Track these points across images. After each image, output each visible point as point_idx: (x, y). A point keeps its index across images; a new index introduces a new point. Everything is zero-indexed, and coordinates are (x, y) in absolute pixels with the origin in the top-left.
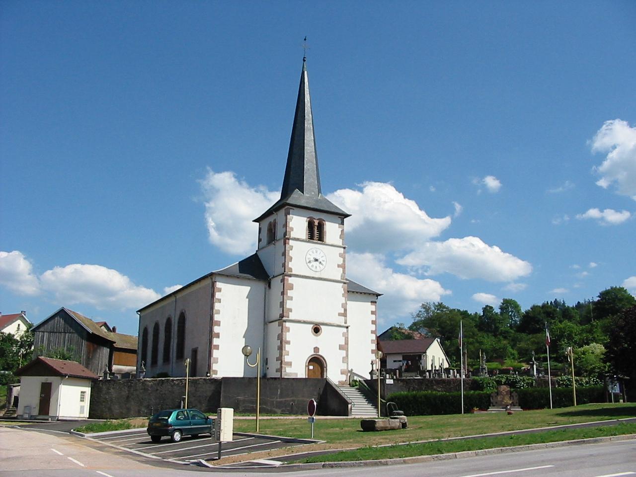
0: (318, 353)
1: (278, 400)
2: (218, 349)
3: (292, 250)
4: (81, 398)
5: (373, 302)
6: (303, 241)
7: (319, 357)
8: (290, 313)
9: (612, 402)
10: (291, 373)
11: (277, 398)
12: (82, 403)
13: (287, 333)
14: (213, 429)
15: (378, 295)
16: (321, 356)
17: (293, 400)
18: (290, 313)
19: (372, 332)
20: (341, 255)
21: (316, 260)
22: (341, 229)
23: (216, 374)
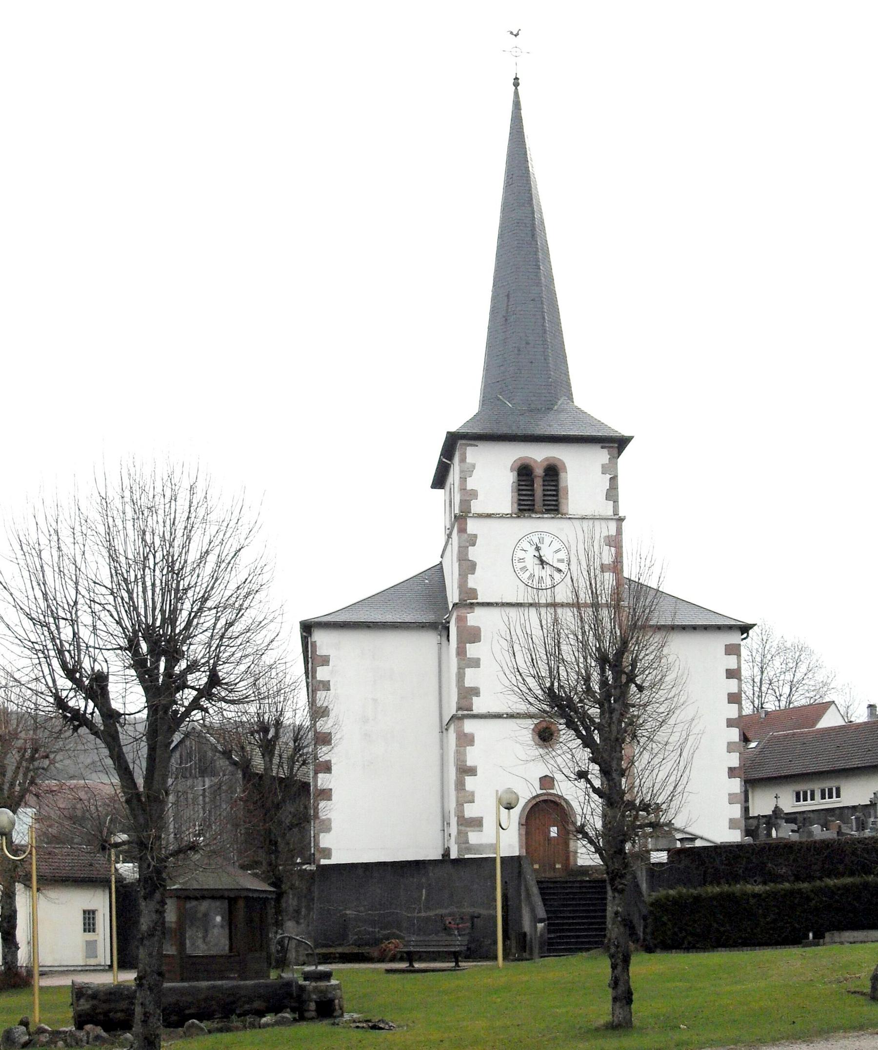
0: (551, 791)
1: (423, 914)
2: (731, 820)
3: (474, 545)
4: (89, 932)
5: (733, 650)
6: (502, 517)
7: (557, 799)
8: (475, 699)
9: (825, 798)
10: (481, 845)
11: (419, 912)
12: (90, 936)
13: (468, 748)
14: (808, 937)
15: (745, 629)
16: (561, 797)
17: (451, 914)
18: (475, 699)
19: (730, 723)
20: (474, 494)
21: (542, 562)
22: (608, 476)
23: (329, 857)
